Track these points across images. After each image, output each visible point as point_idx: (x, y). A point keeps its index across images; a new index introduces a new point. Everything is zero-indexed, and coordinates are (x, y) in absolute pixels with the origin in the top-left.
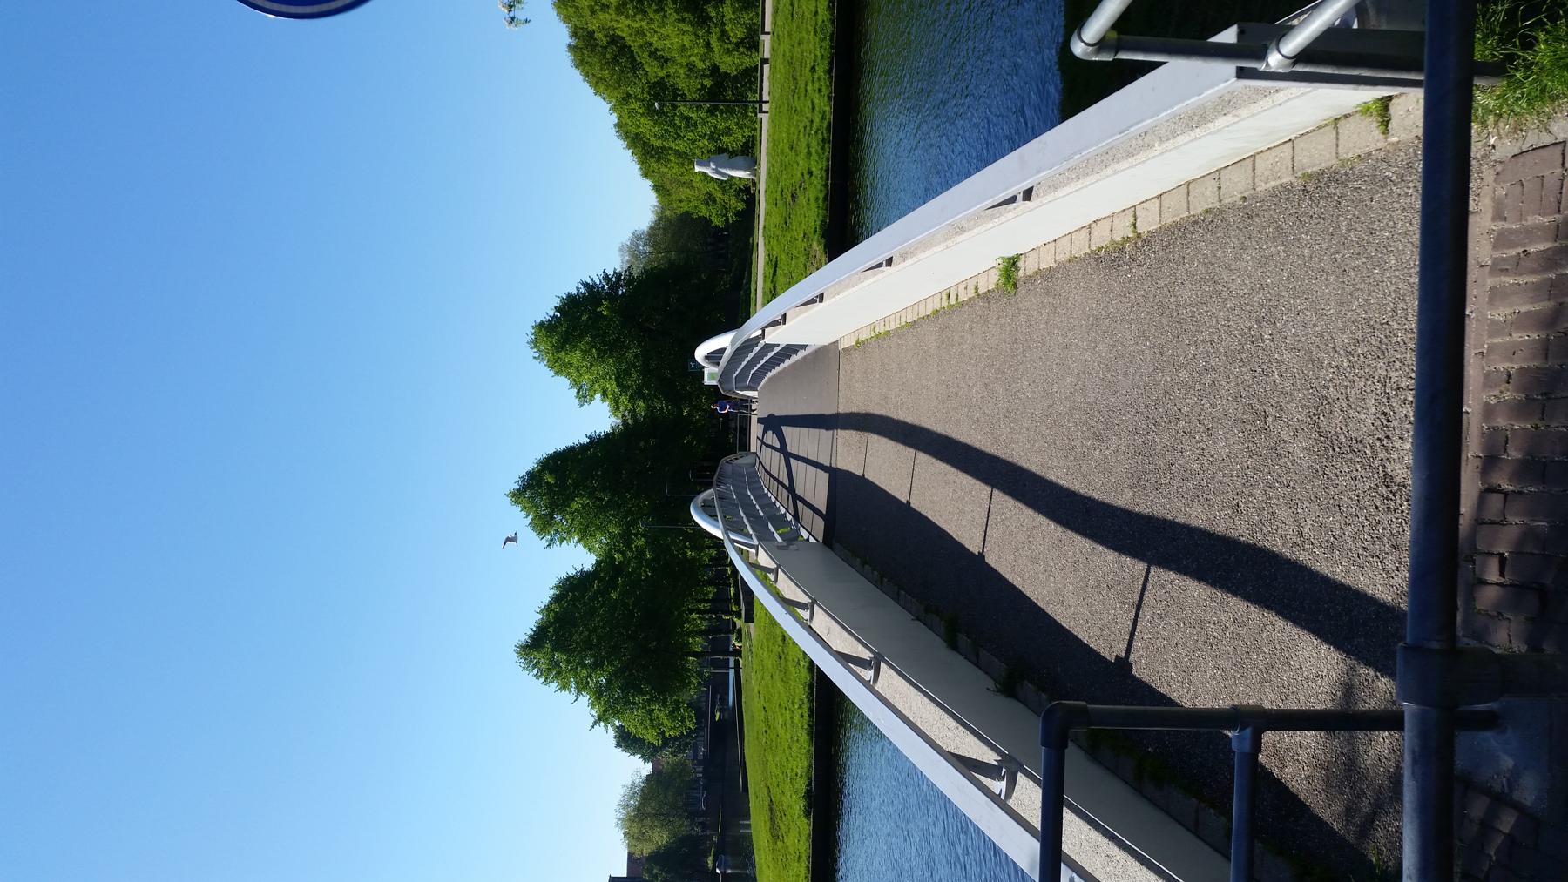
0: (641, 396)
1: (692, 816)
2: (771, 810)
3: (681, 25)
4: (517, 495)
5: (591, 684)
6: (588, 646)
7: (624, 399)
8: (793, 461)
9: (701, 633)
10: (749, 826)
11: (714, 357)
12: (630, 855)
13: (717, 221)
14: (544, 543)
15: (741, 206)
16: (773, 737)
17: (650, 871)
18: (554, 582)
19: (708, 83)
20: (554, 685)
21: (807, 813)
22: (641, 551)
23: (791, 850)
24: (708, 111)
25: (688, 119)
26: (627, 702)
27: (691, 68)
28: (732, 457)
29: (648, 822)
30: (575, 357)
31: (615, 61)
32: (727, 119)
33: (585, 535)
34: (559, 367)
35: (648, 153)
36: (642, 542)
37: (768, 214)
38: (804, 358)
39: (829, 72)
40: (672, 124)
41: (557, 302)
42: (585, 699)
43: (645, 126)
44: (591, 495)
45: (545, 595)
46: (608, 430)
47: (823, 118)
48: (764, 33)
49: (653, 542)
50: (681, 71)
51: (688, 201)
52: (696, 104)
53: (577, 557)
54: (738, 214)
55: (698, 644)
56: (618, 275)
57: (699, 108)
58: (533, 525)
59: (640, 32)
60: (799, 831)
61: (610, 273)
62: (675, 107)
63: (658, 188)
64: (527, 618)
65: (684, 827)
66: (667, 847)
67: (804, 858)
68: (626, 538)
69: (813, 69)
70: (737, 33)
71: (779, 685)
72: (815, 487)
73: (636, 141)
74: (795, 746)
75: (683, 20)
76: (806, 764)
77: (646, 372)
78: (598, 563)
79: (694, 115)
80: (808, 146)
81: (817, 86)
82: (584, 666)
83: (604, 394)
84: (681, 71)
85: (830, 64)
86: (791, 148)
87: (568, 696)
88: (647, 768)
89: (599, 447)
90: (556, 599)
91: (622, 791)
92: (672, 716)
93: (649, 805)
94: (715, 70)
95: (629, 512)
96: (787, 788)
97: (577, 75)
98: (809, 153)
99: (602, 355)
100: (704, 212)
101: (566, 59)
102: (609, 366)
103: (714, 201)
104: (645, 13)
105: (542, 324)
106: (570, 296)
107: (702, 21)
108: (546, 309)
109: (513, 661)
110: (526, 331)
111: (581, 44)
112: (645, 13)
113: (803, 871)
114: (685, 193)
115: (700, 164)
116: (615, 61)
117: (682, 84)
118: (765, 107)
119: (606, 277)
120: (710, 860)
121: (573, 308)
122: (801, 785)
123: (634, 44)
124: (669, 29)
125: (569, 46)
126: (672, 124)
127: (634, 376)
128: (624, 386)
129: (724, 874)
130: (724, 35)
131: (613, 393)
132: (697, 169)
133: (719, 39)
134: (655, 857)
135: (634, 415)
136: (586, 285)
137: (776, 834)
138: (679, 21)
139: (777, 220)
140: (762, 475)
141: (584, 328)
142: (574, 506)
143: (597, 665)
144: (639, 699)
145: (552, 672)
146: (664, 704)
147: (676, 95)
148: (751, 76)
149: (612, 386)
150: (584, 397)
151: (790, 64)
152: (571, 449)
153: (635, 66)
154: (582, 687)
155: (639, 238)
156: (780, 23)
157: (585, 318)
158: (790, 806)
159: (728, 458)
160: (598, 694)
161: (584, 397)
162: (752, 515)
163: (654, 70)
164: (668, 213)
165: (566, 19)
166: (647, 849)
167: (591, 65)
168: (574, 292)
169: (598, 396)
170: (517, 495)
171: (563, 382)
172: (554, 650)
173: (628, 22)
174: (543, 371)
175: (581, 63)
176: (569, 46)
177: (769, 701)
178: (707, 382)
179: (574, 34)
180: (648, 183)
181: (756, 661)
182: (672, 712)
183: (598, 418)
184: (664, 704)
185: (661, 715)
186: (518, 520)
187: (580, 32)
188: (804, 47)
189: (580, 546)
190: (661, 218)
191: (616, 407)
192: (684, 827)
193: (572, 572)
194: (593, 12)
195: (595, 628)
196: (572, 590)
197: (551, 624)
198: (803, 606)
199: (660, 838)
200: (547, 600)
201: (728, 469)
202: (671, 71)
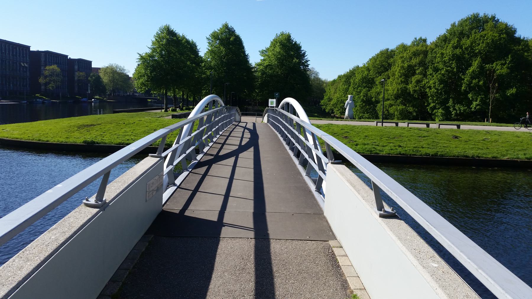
0: (263, 74)
1: (114, 91)
2: (91, 125)
3: (396, 90)
4: (226, 26)
5: (154, 54)
6: (169, 52)
7: (261, 67)
8: (233, 159)
9: (175, 96)
10: (100, 114)
11: (289, 107)
12: (99, 69)
13: (322, 102)
14: (208, 37)
15: (327, 111)
16: (121, 127)
17: (94, 76)
18: (195, 41)
19: (373, 99)
20: (154, 39)
21: (85, 142)
22: (205, 73)
23: (72, 134)
24: (363, 99)
25: (360, 92)
26: (148, 67)
27: (379, 94)
28: (239, 111)
29: (111, 75)
30: (278, 49)
31: (382, 66)
32: (360, 106)
33: (211, 52)
34: (274, 43)
35: (347, 78)
36: (208, 73)
37: (338, 126)
38: (282, 144)
39: (400, 154)
40: (359, 86)
41: (298, 42)
42: (149, 51)
43: (358, 77)
44: (226, 55)
45: (190, 37)
46: (250, 62)
47: (380, 151)
48: (408, 124)
49: (208, 78)
50: (378, 90)
51: (330, 92)
52: (366, 95)
53: (203, 49)
54: (324, 110)
55: (170, 94)
56: (308, 66)
57: (364, 96)
58: (215, 32)
59: (394, 75)
60: (78, 138)
61: (309, 63)
62: (365, 87)
63: (334, 81)
64: (180, 30)
65: (109, 88)
66: (102, 82)
67: (67, 140)
68: (210, 68)
69: (400, 146)
70: (391, 110)
71: (143, 130)
72: (205, 208)
73: (352, 74)
74: (116, 137)
75: (398, 90)
76: (107, 141)
77: (271, 76)
78: (201, 57)
79: (362, 94)
80: (368, 144)
81: (394, 148)
82: (161, 51)
83: (264, 60)
84: (378, 90)
85: (403, 154)
86: (366, 136)
87: (150, 45)
88: (131, 75)
89: (244, 58)
90: (187, 41)
91: (122, 66)
92: (143, 84)
93: (118, 76)
94: (378, 102)
95: (220, 69)
96: (99, 133)
97: (377, 51)
98: (365, 144)
99: (278, 59)
100: (326, 98)
101: (383, 48)
102: (275, 62)
103: (329, 101)
104: (401, 77)
105: (290, 36)
106: (300, 47)
107: (397, 97)
108: (296, 38)
109: (163, 24)
110: (286, 31)
111: (389, 53)
112: (401, 77)
113: (61, 140)
114: (333, 91)
115: (351, 97)
116: (382, 66)
117: (374, 90)
118: (380, 124)
119: (307, 61)
120: (98, 97)
121: (297, 48)
122: (99, 139)
123: (390, 72)
124: (395, 85)
125: (388, 49)
126: (359, 86)
127: (270, 72)
128: (266, 67)
129: (92, 102)
130: (391, 105)
131: (264, 64)
132: (349, 96)
133: (390, 104)
134: (99, 78)
135: (255, 71)
136: (304, 53)
137: (80, 127)
138: (398, 89)
139: (336, 130)
140: (230, 127)
141: (289, 53)
142: (222, 48)
143: (162, 56)
144: (148, 72)
145: (159, 38)
146: (147, 81)
147: (369, 87)
148: (374, 116)
149: (266, 63)
150: (263, 53)
151: (400, 136)
152: (243, 48)
153: (380, 73)
154: (154, 50)
155: (316, 74)
156: (416, 131)
157: (292, 53)
158: (90, 134)
159: (238, 109)
160: (151, 56)
161: (263, 53)
162: (201, 134)
163: (379, 79)
164: (325, 85)
165: (397, 48)
166: (101, 75)
167: (381, 57)
168: (302, 49)
169: (262, 58)
170: (226, 26)
171: (268, 45)
172: (167, 39)
173: (398, 70)
174: (272, 37)
175: (382, 53)
176: (388, 49)
177: (137, 125)
178: (270, 100)
179: (392, 51)
180: (335, 77)
181: (154, 119)
182: (143, 84)
183: (255, 58)
184: (147, 81)
185: (143, 80)
186: (217, 27)
187: (393, 53)
188: (408, 142)
189: (207, 50)
190: (323, 82)
191: (259, 65)
192: (109, 88)
193: (198, 48)
194: (402, 57)
195: (176, 56)
196: (192, 47)
197: (177, 38)
198: (100, 196)
199: (105, 79)
200: (187, 38)
201: (233, 112)
202: (378, 86)
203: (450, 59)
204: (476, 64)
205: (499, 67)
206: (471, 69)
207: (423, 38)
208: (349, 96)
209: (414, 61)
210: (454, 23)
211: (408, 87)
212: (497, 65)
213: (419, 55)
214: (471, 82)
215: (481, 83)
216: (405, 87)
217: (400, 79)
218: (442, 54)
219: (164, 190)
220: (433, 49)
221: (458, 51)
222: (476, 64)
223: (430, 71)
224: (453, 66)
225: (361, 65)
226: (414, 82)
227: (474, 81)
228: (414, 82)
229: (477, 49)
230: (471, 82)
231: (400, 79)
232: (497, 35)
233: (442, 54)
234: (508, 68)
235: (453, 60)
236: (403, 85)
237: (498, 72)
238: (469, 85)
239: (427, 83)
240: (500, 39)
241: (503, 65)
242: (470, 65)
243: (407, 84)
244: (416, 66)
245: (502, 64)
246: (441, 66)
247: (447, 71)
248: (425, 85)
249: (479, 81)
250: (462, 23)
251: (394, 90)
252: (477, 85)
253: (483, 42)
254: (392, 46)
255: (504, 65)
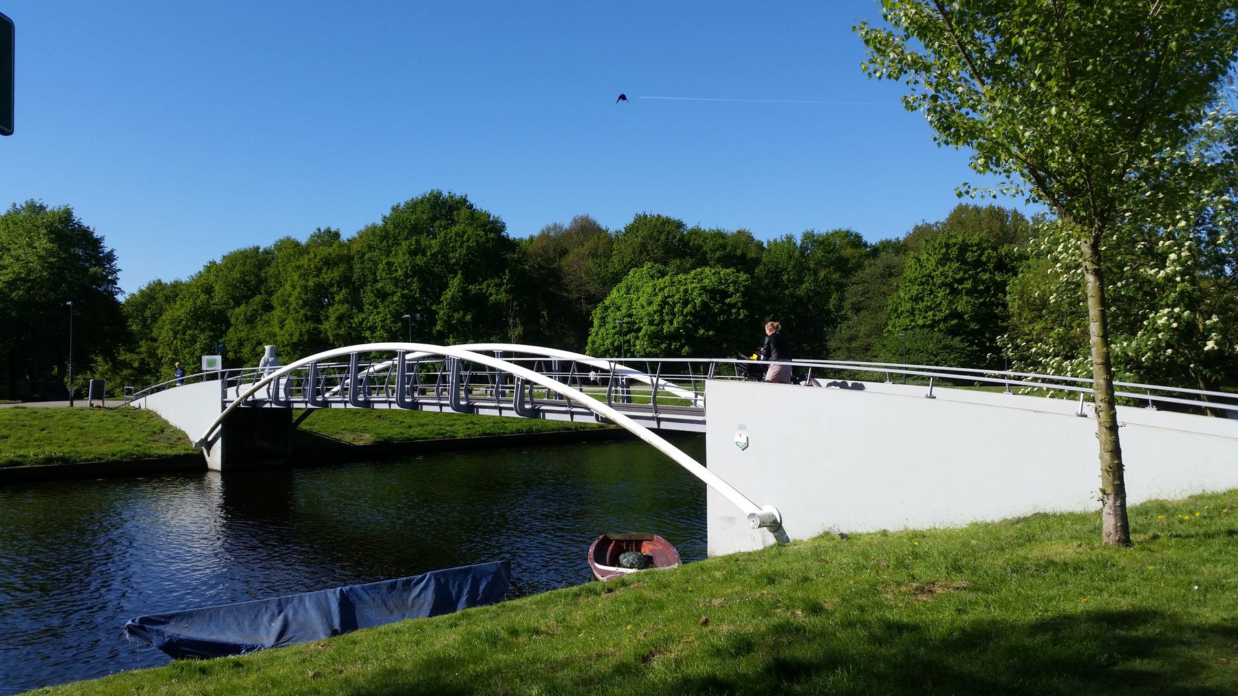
50: (243, 334)
62: (203, 330)
75: (301, 335)
98: (422, 425)
121: (89, 242)
124: (290, 324)
132: (267, 348)
178: (205, 358)
179: (267, 252)
203: (406, 275)
204: (455, 283)
205: (493, 290)
206: (448, 295)
207: (333, 229)
208: (267, 348)
209: (328, 276)
210: (398, 206)
211: (322, 327)
212: (488, 286)
213: (337, 264)
214: (450, 317)
215: (468, 317)
216: (315, 329)
217: (302, 312)
218: (389, 264)
219: (613, 427)
220: (364, 254)
221: (420, 260)
222: (455, 283)
223: (368, 297)
224: (414, 286)
225: (184, 279)
226: (333, 318)
227: (456, 315)
228: (333, 318)
229: (454, 257)
230: (450, 317)
231: (302, 312)
232: (482, 233)
233: (389, 264)
234: (507, 292)
235: (413, 277)
236: (310, 325)
237: (492, 298)
238: (447, 323)
239: (364, 319)
240: (488, 240)
241: (499, 285)
242: (445, 286)
243: (319, 321)
244: (332, 285)
245: (496, 285)
246: (390, 288)
247: (403, 296)
248: (361, 323)
249: (465, 315)
250: (414, 206)
251: (291, 335)
252: (461, 321)
253: (461, 246)
254: (266, 242)
255: (500, 285)
